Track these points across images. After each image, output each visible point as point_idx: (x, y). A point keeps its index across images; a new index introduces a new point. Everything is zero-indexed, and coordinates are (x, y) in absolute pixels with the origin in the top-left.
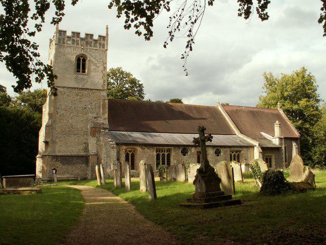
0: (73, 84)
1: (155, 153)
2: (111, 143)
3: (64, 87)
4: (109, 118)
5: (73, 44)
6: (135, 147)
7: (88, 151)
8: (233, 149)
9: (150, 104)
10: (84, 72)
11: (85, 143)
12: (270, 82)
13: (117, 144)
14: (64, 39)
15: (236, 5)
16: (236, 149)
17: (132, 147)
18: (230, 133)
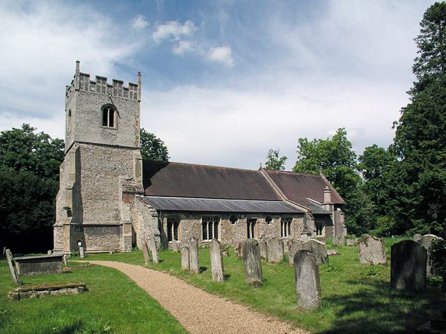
0: (98, 139)
1: (201, 221)
2: (151, 209)
3: (88, 143)
4: (143, 181)
5: (98, 90)
6: (179, 214)
7: (120, 220)
8: (284, 216)
9: (150, 181)
10: (111, 125)
11: (116, 210)
12: (304, 145)
13: (158, 211)
14: (87, 85)
15: (11, 265)
16: (288, 216)
17: (175, 214)
18: (273, 197)
